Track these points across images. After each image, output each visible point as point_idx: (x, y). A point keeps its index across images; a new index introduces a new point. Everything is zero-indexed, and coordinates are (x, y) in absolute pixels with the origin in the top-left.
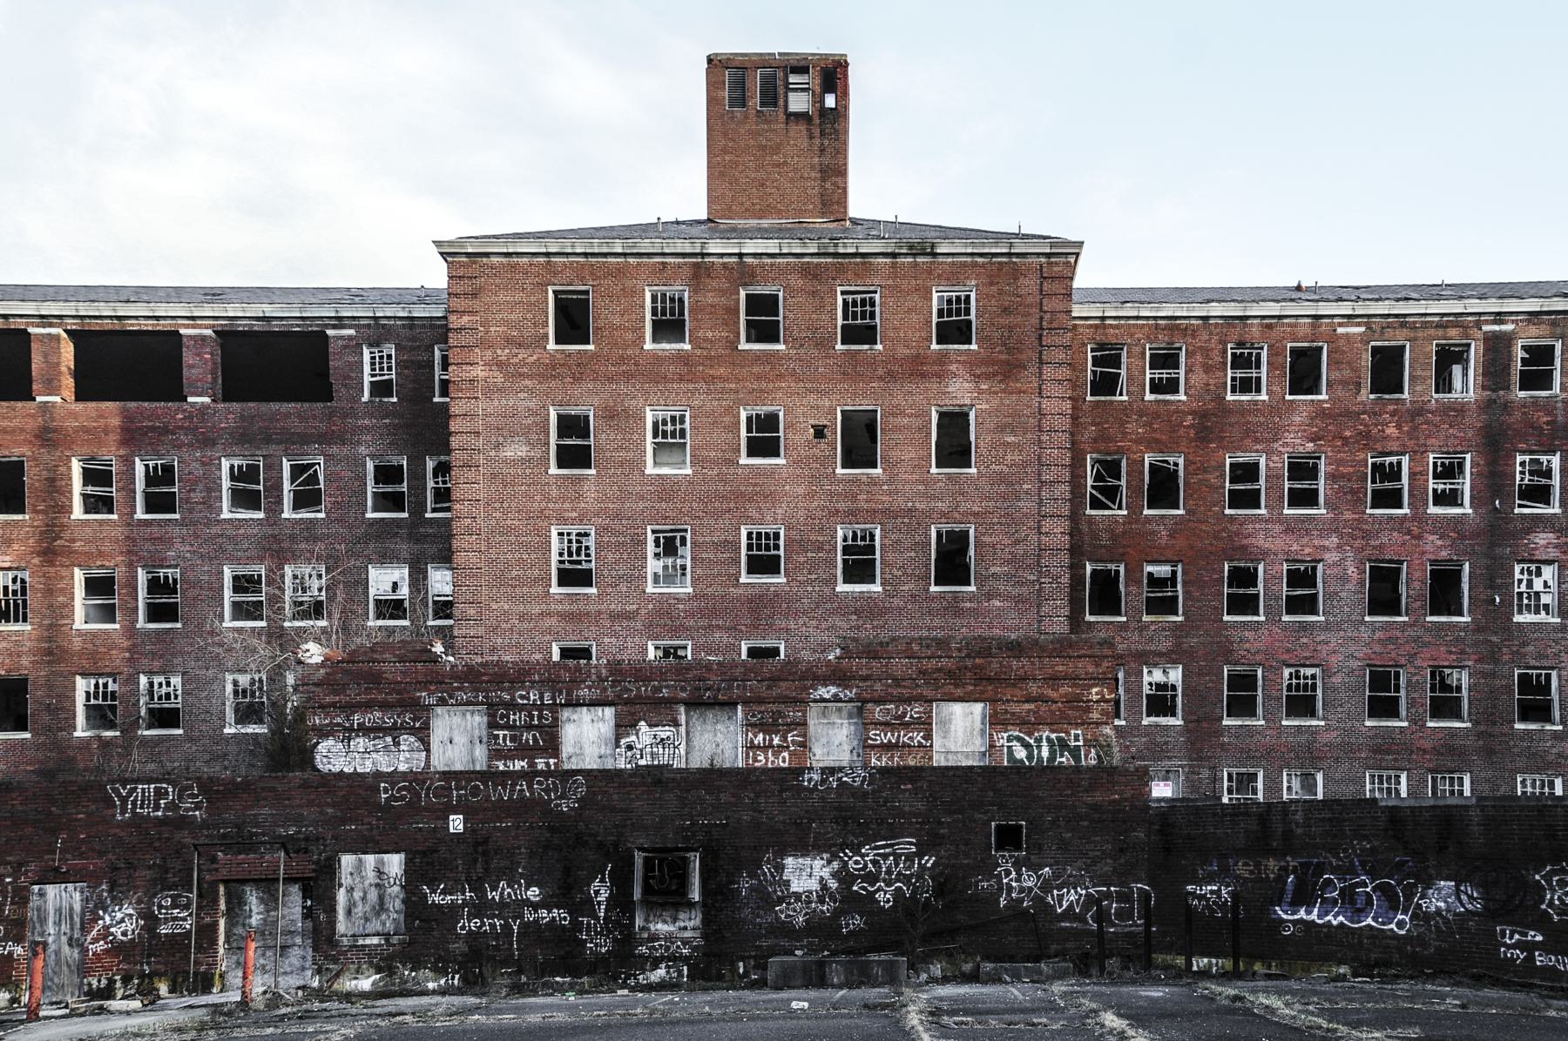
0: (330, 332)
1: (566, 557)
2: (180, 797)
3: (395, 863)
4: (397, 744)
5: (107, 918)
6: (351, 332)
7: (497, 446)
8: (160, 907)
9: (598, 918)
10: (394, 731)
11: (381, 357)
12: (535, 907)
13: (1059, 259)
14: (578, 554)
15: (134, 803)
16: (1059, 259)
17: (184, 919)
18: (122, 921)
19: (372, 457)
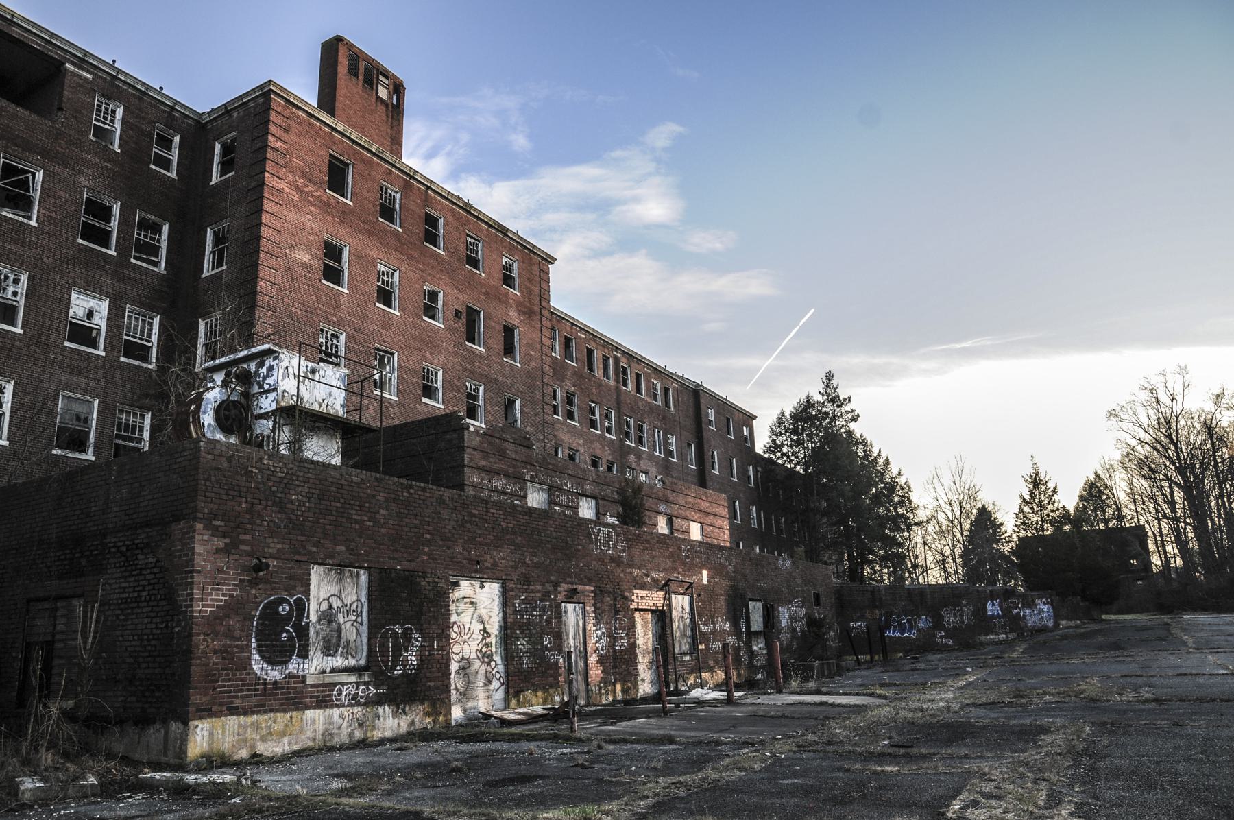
6: (90, 77)
7: (291, 247)
11: (107, 109)
19: (90, 189)
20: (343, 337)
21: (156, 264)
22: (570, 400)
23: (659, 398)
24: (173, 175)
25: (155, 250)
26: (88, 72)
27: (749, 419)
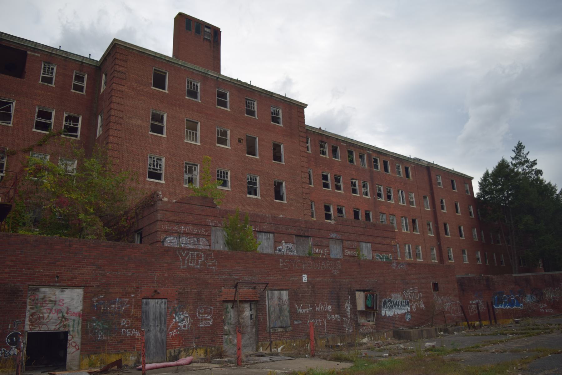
0: (28, 52)
1: (152, 167)
2: (207, 259)
3: (285, 294)
4: (198, 241)
5: (177, 318)
6: (39, 55)
8: (199, 313)
9: (348, 318)
10: (198, 235)
12: (331, 314)
13: (301, 107)
14: (157, 167)
15: (188, 260)
16: (301, 107)
17: (209, 320)
18: (183, 320)
20: (164, 160)
21: (76, 136)
22: (337, 180)
23: (401, 173)
24: (84, 93)
25: (75, 130)
26: (39, 53)
27: (470, 179)
